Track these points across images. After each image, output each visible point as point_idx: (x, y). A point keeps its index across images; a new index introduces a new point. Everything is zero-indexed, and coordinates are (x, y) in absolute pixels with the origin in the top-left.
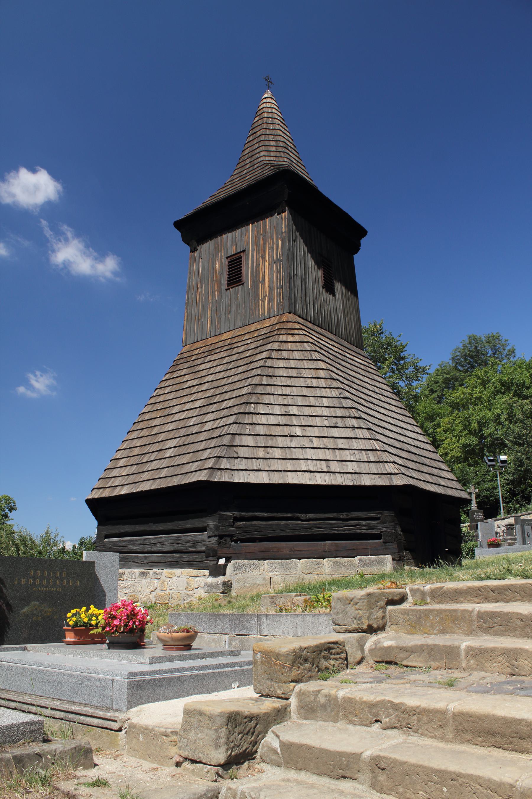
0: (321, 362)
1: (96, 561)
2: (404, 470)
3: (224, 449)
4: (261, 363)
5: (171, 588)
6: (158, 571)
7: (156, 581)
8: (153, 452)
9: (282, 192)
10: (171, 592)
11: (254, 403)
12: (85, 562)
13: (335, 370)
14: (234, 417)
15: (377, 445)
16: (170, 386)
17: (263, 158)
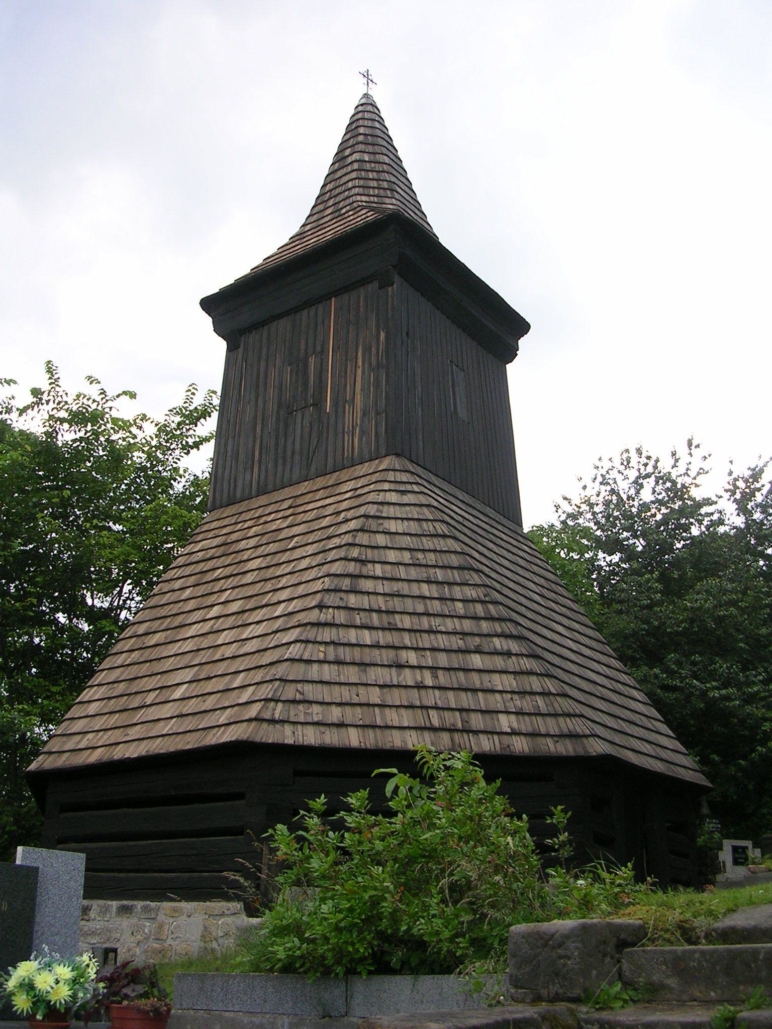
1: (41, 866)
2: (599, 730)
3: (279, 686)
5: (174, 936)
6: (153, 904)
10: (173, 943)
11: (334, 607)
12: (19, 866)
13: (477, 555)
14: (298, 630)
15: (551, 686)
16: (183, 577)
17: (359, 198)
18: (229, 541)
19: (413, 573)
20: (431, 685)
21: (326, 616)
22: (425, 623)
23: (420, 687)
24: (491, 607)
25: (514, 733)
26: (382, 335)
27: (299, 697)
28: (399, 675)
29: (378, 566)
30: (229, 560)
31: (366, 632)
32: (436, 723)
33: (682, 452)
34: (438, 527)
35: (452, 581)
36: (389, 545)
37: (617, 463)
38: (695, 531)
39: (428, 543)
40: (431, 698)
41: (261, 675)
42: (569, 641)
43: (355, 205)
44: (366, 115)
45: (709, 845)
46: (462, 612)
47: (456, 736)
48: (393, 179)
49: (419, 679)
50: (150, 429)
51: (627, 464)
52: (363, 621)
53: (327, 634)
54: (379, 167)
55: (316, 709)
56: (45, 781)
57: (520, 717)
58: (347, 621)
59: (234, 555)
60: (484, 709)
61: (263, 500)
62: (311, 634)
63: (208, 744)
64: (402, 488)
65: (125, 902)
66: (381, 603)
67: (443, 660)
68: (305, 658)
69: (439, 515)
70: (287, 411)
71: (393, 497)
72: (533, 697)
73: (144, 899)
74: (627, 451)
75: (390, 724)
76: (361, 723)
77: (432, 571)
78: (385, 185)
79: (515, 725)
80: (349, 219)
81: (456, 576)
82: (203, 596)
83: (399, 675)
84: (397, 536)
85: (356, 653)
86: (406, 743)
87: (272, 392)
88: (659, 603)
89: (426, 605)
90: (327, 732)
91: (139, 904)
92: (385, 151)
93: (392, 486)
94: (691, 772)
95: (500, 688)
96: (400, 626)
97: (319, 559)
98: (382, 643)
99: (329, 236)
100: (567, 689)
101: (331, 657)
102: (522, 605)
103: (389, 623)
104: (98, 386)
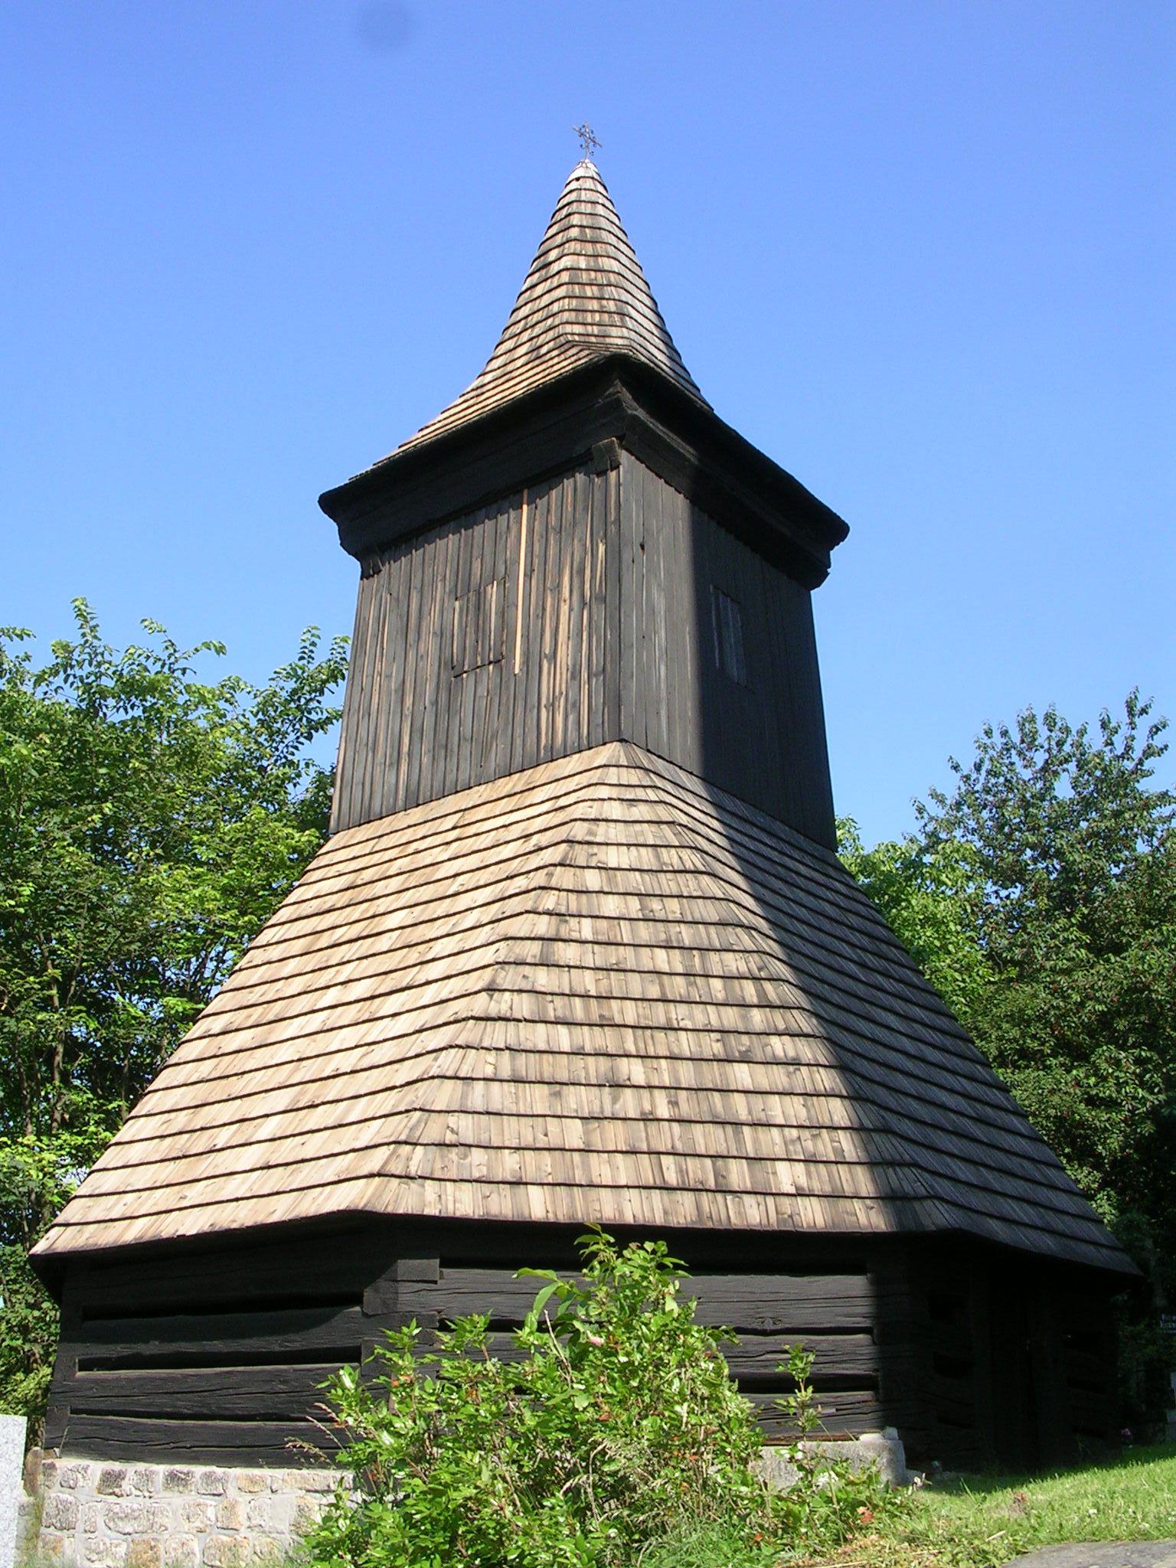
0: (706, 877)
2: (944, 1187)
4: (539, 879)
7: (211, 1501)
8: (181, 1133)
9: (605, 412)
17: (568, 328)
18: (360, 882)
19: (645, 933)
20: (667, 1116)
21: (502, 1004)
22: (659, 1014)
23: (648, 1118)
24: (767, 985)
25: (800, 1193)
26: (602, 548)
27: (450, 1138)
28: (615, 1100)
29: (586, 923)
30: (356, 913)
31: (562, 1030)
32: (672, 1179)
33: (1119, 716)
34: (685, 858)
35: (706, 945)
36: (606, 889)
37: (1016, 737)
38: (1142, 848)
39: (668, 884)
40: (667, 1136)
41: (392, 1102)
42: (904, 1039)
43: (562, 340)
44: (584, 195)
45: (1165, 1358)
46: (720, 996)
47: (705, 1198)
48: (626, 297)
49: (647, 1107)
50: (247, 703)
51: (1030, 741)
52: (560, 1013)
53: (498, 1035)
54: (601, 278)
55: (478, 1156)
56: (59, 1274)
57: (812, 1166)
58: (532, 1013)
59: (366, 905)
60: (752, 1155)
61: (416, 814)
62: (468, 1033)
63: (303, 1215)
64: (629, 794)
65: (178, 1467)
66: (588, 982)
67: (686, 1074)
68: (462, 1074)
69: (690, 838)
70: (454, 671)
71: (615, 810)
72: (834, 1134)
73: (206, 1463)
74: (1032, 719)
75: (596, 1181)
76: (550, 1180)
77: (674, 929)
78: (611, 306)
79: (803, 1181)
80: (550, 363)
81: (714, 936)
82: (313, 971)
83: (615, 1100)
84: (618, 873)
85: (545, 1064)
86: (621, 1213)
87: (430, 645)
88: (1080, 965)
89: (662, 985)
90: (494, 1196)
91: (199, 1470)
92: (612, 251)
93: (614, 792)
94: (1105, 1251)
95: (780, 1121)
96: (618, 1020)
97: (494, 911)
98: (588, 1049)
99: (519, 391)
100: (893, 1121)
101: (506, 1073)
102: (822, 981)
103: (601, 1016)
104: (162, 637)
